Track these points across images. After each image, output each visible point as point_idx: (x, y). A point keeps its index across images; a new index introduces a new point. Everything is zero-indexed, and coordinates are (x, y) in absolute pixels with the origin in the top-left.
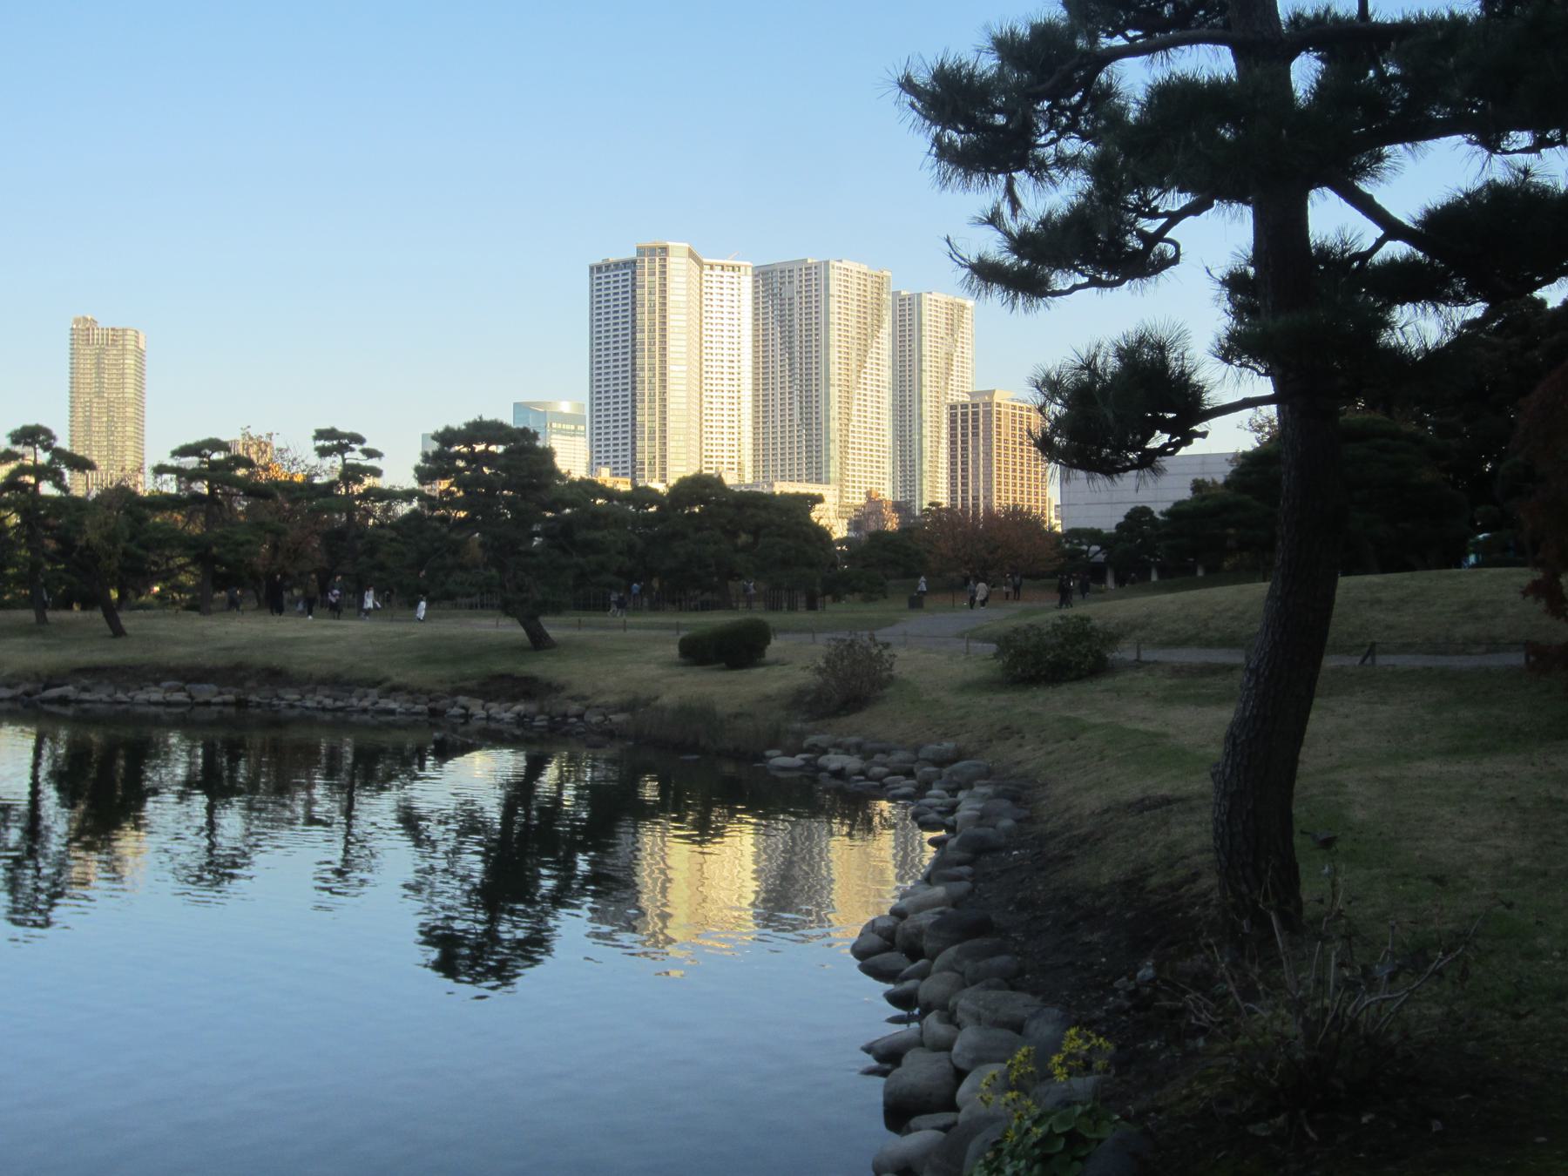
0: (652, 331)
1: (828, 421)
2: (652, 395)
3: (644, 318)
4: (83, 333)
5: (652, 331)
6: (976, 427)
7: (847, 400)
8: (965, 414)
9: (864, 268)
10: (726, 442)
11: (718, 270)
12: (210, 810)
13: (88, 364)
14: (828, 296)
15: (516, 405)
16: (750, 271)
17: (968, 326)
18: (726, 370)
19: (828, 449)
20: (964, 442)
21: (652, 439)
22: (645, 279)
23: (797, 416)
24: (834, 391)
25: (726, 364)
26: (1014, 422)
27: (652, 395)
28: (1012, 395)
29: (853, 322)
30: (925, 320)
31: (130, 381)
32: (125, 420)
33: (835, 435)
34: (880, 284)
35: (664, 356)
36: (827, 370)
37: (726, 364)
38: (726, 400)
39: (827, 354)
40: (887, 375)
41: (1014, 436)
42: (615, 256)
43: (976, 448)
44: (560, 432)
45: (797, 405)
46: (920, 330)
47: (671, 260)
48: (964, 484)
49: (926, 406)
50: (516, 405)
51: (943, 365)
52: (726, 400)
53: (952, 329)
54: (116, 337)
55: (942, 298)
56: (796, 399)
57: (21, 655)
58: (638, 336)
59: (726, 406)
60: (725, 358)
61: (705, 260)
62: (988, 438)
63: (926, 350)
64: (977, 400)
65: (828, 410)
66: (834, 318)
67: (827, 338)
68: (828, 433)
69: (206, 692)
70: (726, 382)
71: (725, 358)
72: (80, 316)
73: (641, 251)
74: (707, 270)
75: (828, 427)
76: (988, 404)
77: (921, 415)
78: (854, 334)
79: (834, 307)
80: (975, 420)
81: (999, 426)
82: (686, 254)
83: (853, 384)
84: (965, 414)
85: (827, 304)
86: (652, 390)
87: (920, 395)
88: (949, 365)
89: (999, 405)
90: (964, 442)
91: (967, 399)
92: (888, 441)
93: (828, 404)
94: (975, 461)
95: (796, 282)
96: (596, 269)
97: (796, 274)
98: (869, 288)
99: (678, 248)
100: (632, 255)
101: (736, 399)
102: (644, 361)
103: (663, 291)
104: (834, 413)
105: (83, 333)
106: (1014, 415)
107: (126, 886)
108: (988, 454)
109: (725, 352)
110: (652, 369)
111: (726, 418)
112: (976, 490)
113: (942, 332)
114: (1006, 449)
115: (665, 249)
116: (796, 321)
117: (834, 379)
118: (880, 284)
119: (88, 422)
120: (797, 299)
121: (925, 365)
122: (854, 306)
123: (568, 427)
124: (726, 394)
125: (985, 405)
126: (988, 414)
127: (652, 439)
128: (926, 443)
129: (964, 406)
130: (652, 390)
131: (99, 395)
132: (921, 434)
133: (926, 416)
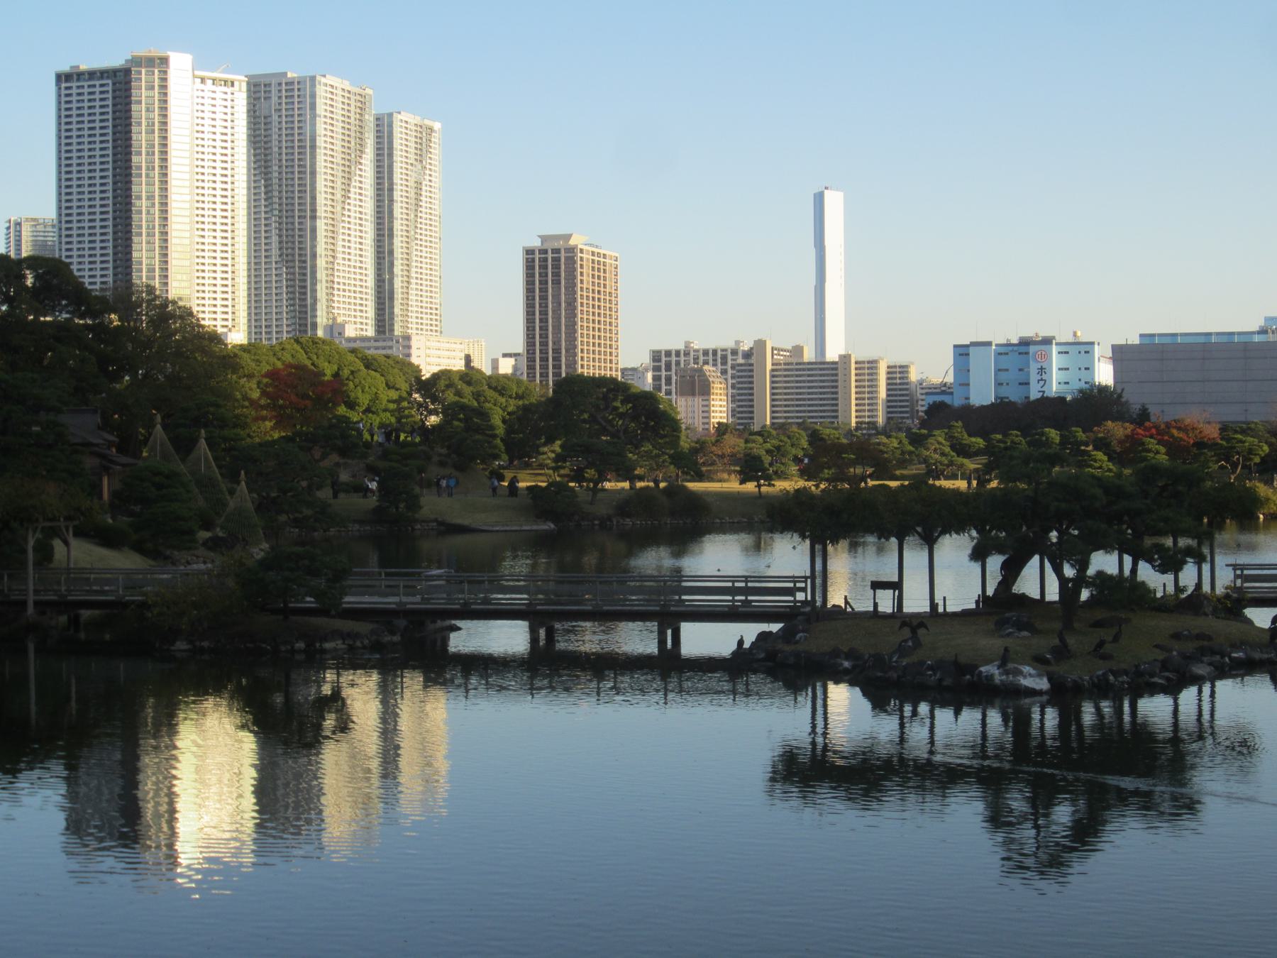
3: (140, 137)
6: (557, 275)
14: (314, 116)
17: (436, 151)
19: (314, 291)
20: (544, 290)
22: (143, 94)
23: (275, 252)
24: (321, 225)
29: (338, 148)
36: (314, 198)
40: (369, 206)
45: (275, 239)
51: (412, 195)
53: (420, 157)
55: (413, 119)
64: (556, 245)
66: (320, 142)
67: (313, 165)
69: (638, 639)
83: (338, 216)
84: (556, 260)
85: (314, 125)
88: (418, 194)
89: (582, 251)
95: (274, 99)
97: (274, 89)
99: (180, 64)
106: (593, 261)
107: (1201, 829)
108: (571, 305)
110: (150, 197)
112: (557, 342)
115: (164, 61)
116: (275, 143)
120: (275, 117)
126: (571, 261)
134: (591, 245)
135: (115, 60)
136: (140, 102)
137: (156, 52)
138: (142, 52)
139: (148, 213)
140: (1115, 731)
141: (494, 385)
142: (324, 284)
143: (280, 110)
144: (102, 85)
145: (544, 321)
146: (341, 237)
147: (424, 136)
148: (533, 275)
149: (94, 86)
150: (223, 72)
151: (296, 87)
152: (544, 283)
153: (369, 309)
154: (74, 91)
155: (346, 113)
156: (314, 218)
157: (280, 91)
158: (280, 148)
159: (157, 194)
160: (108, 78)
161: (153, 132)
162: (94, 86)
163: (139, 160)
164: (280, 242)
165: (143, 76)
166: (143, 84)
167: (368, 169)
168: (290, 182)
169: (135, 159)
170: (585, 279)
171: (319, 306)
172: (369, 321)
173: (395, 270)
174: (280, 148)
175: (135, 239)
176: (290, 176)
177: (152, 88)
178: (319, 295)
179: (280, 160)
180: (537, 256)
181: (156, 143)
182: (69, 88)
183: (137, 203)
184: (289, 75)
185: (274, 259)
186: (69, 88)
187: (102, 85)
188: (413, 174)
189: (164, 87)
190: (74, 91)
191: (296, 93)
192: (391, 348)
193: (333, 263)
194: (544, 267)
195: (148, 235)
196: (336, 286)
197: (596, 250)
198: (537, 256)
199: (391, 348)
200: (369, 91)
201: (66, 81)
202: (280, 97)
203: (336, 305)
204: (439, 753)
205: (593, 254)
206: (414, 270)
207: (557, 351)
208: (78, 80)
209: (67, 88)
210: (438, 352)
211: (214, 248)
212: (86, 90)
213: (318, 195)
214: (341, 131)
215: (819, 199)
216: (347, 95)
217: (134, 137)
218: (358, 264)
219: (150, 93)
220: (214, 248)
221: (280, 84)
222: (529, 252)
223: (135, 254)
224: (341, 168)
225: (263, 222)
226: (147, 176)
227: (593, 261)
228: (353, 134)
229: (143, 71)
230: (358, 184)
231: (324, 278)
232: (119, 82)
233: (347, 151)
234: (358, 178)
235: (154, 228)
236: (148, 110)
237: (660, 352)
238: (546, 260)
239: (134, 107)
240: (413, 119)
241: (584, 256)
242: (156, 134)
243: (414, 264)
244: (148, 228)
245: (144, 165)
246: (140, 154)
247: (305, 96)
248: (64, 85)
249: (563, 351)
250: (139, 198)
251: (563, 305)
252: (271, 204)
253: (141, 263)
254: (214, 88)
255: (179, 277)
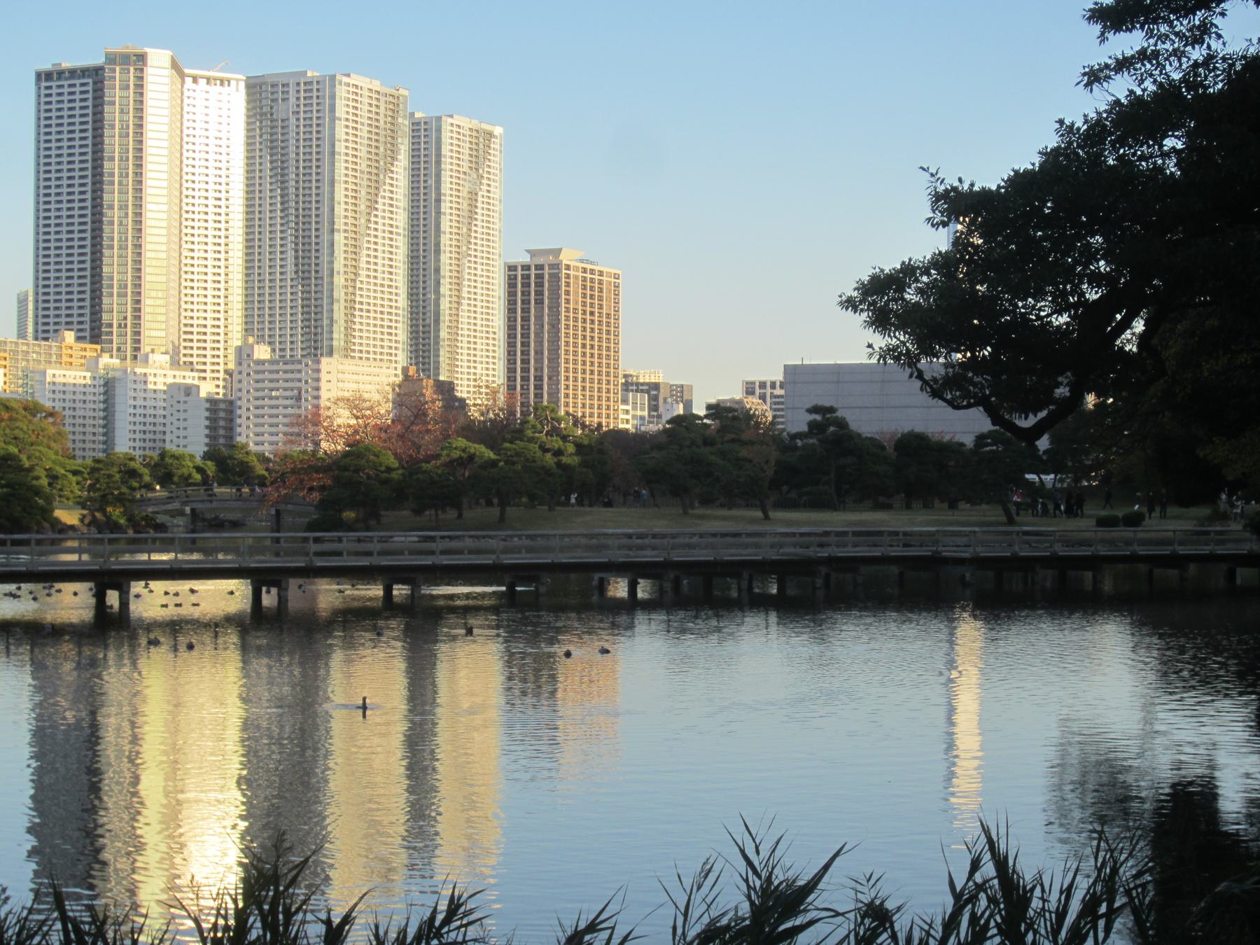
1: (332, 275)
3: (113, 142)
6: (539, 293)
8: (540, 277)
9: (376, 85)
10: (210, 300)
11: (203, 82)
14: (333, 119)
16: (242, 85)
17: (496, 158)
18: (211, 209)
20: (526, 311)
21: (122, 295)
22: (116, 94)
23: (290, 268)
24: (339, 238)
25: (211, 202)
26: (584, 287)
28: (580, 255)
29: (363, 153)
30: (445, 150)
33: (339, 294)
34: (395, 105)
35: (139, 190)
37: (211, 202)
38: (210, 247)
39: (332, 192)
40: (402, 219)
41: (584, 304)
43: (539, 318)
46: (438, 163)
48: (525, 362)
49: (444, 258)
51: (465, 206)
52: (210, 247)
55: (466, 123)
56: (290, 246)
58: (107, 165)
59: (210, 255)
60: (211, 194)
61: (187, 71)
62: (555, 307)
63: (446, 187)
64: (540, 261)
66: (340, 147)
70: (211, 224)
71: (211, 194)
73: (112, 59)
74: (189, 80)
76: (556, 266)
77: (437, 270)
78: (364, 167)
79: (340, 132)
80: (540, 284)
81: (568, 293)
82: (168, 64)
83: (362, 230)
84: (540, 277)
85: (333, 129)
87: (438, 244)
89: (568, 267)
90: (526, 311)
91: (526, 259)
92: (402, 301)
93: (332, 253)
94: (539, 334)
95: (292, 100)
96: (44, 77)
97: (292, 90)
98: (382, 111)
99: (159, 60)
100: (99, 60)
101: (222, 246)
102: (112, 196)
104: (339, 265)
106: (584, 279)
109: (211, 187)
110: (123, 207)
111: (210, 270)
112: (539, 369)
114: (576, 319)
115: (142, 58)
116: (292, 149)
117: (339, 224)
120: (293, 121)
121: (445, 207)
124: (210, 240)
125: (552, 266)
126: (555, 278)
127: (122, 295)
128: (445, 304)
129: (526, 267)
132: (437, 292)
133: (445, 270)
134: (582, 261)
136: (114, 103)
137: (132, 48)
139: (121, 224)
140: (12, 647)
142: (343, 303)
143: (298, 113)
145: (525, 344)
146: (365, 252)
149: (74, 85)
150: (220, 71)
152: (526, 302)
153: (399, 332)
154: (54, 91)
157: (298, 91)
158: (297, 154)
160: (89, 77)
162: (74, 85)
164: (296, 258)
165: (117, 75)
166: (117, 83)
167: (401, 177)
170: (572, 299)
171: (335, 328)
173: (442, 290)
174: (297, 154)
175: (106, 252)
176: (307, 185)
180: (519, 272)
184: (309, 74)
185: (289, 277)
187: (82, 85)
189: (140, 86)
192: (300, 371)
193: (354, 281)
194: (526, 285)
195: (120, 248)
196: (357, 306)
197: (589, 267)
198: (519, 272)
199: (300, 371)
200: (403, 92)
201: (46, 80)
202: (298, 99)
203: (357, 327)
205: (585, 271)
207: (539, 378)
208: (59, 79)
209: (47, 88)
210: (355, 377)
212: (66, 90)
214: (366, 135)
215: (81, 119)
216: (375, 96)
217: (107, 141)
218: (386, 283)
219: (125, 93)
221: (298, 84)
225: (279, 235)
226: (120, 183)
227: (584, 279)
228: (382, 139)
229: (132, 69)
230: (388, 194)
234: (387, 187)
235: (126, 240)
236: (122, 112)
237: (753, 383)
238: (529, 277)
239: (107, 108)
240: (466, 123)
241: (571, 272)
243: (466, 283)
244: (120, 240)
247: (324, 97)
249: (546, 379)
250: (111, 207)
251: (546, 327)
252: (287, 216)
254: (208, 88)
255: (153, 294)
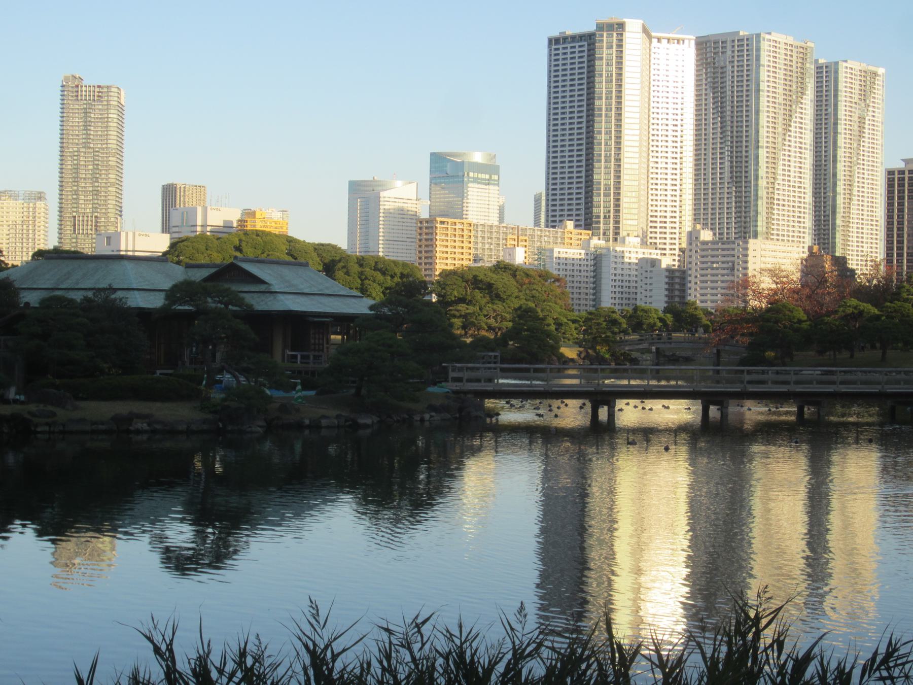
0: (609, 98)
2: (608, 157)
3: (601, 86)
4: (71, 90)
5: (609, 98)
7: (774, 161)
9: (790, 40)
11: (664, 42)
12: (682, 429)
13: (76, 118)
14: (758, 66)
15: (432, 154)
17: (879, 91)
18: (670, 133)
19: (756, 206)
21: (607, 195)
22: (604, 52)
23: (727, 175)
24: (763, 153)
25: (670, 128)
27: (608, 157)
29: (780, 90)
30: (841, 86)
31: (113, 133)
32: (108, 168)
34: (804, 54)
35: (619, 120)
36: (757, 132)
37: (670, 128)
38: (670, 160)
39: (757, 119)
40: (808, 138)
42: (573, 29)
44: (476, 180)
46: (836, 96)
47: (628, 37)
50: (432, 154)
51: (856, 128)
52: (670, 160)
54: (101, 93)
55: (856, 65)
56: (727, 159)
57: (908, 305)
59: (670, 166)
61: (653, 34)
63: (841, 114)
65: (757, 170)
66: (763, 86)
68: (756, 191)
72: (68, 74)
73: (601, 27)
74: (655, 41)
75: (757, 185)
77: (835, 175)
78: (781, 101)
82: (640, 29)
83: (779, 146)
85: (758, 73)
86: (608, 151)
91: (902, 165)
92: (809, 198)
93: (757, 163)
95: (729, 53)
96: (554, 42)
97: (729, 45)
99: (633, 27)
101: (678, 159)
102: (601, 125)
103: (620, 63)
104: (762, 172)
105: (71, 90)
110: (608, 133)
111: (669, 177)
113: (856, 98)
115: (621, 26)
117: (763, 142)
118: (804, 54)
119: (76, 168)
120: (729, 68)
121: (841, 128)
122: (781, 74)
123: (483, 176)
127: (607, 195)
129: (902, 172)
130: (608, 151)
131: (86, 145)
132: (834, 191)
135: (588, 27)
136: (602, 59)
137: (614, 18)
138: (605, 19)
139: (606, 144)
141: (380, 266)
143: (733, 62)
144: (580, 46)
146: (781, 162)
147: (868, 80)
148: (893, 192)
149: (574, 47)
150: (677, 33)
151: (745, 42)
154: (561, 52)
155: (788, 63)
156: (757, 147)
157: (733, 46)
158: (732, 92)
159: (613, 130)
161: (611, 81)
162: (574, 47)
163: (601, 103)
164: (731, 167)
165: (605, 38)
166: (605, 44)
168: (739, 119)
169: (597, 103)
172: (807, 231)
174: (732, 92)
175: (596, 165)
176: (739, 114)
177: (611, 47)
178: (760, 209)
179: (732, 102)
181: (614, 90)
182: (558, 49)
183: (598, 137)
184: (741, 33)
186: (558, 49)
187: (580, 46)
188: (857, 111)
190: (561, 52)
191: (745, 48)
192: (733, 249)
193: (773, 183)
198: (907, 175)
199: (733, 249)
200: (810, 44)
201: (556, 44)
202: (733, 52)
203: (775, 217)
204: (322, 564)
206: (856, 189)
209: (556, 49)
210: (774, 254)
211: (666, 171)
212: (569, 51)
213: (761, 129)
214: (783, 77)
216: (789, 48)
217: (597, 85)
219: (610, 51)
220: (666, 171)
221: (733, 41)
222: (890, 173)
223: (595, 177)
224: (782, 107)
226: (606, 115)
228: (794, 79)
229: (605, 34)
231: (765, 195)
232: (589, 41)
233: (788, 93)
234: (798, 115)
236: (608, 64)
238: (903, 179)
240: (856, 65)
242: (614, 84)
244: (606, 156)
245: (604, 107)
246: (601, 98)
247: (752, 50)
248: (553, 47)
250: (600, 133)
253: (600, 183)
255: (629, 194)
